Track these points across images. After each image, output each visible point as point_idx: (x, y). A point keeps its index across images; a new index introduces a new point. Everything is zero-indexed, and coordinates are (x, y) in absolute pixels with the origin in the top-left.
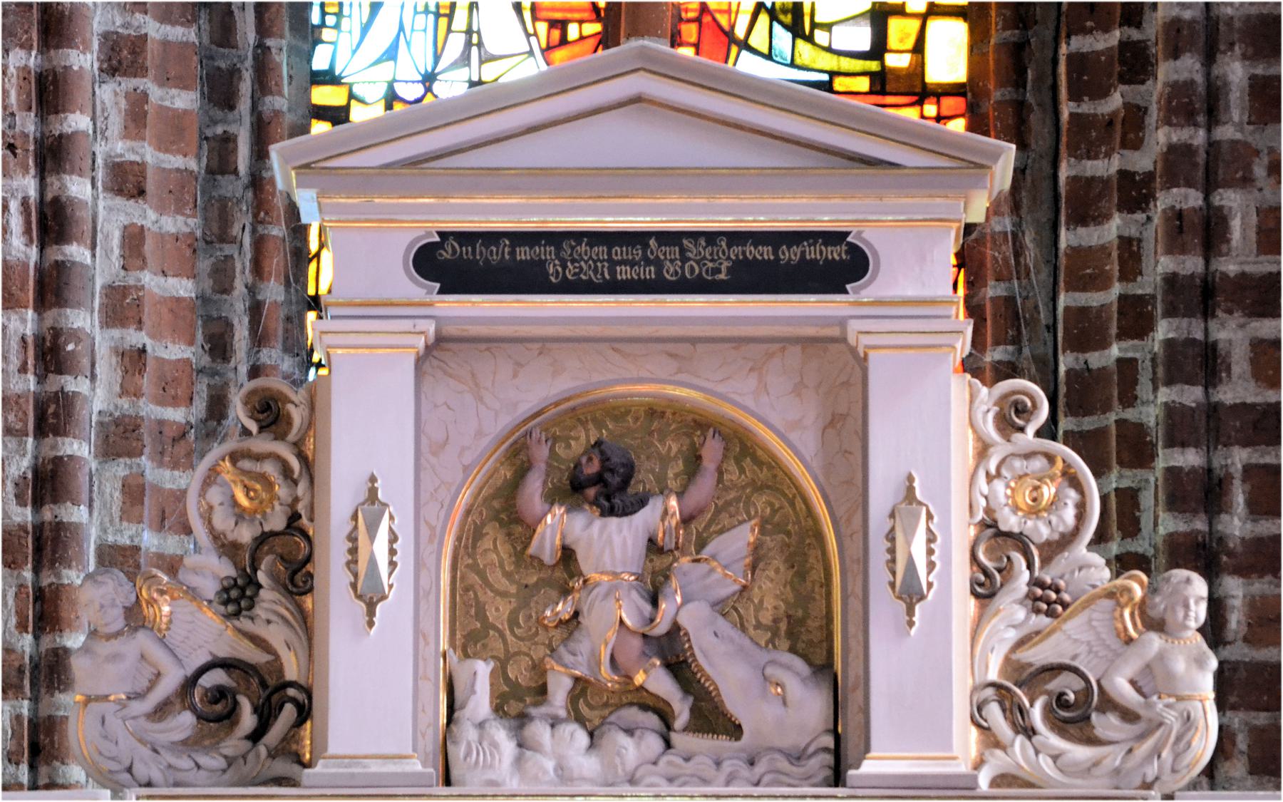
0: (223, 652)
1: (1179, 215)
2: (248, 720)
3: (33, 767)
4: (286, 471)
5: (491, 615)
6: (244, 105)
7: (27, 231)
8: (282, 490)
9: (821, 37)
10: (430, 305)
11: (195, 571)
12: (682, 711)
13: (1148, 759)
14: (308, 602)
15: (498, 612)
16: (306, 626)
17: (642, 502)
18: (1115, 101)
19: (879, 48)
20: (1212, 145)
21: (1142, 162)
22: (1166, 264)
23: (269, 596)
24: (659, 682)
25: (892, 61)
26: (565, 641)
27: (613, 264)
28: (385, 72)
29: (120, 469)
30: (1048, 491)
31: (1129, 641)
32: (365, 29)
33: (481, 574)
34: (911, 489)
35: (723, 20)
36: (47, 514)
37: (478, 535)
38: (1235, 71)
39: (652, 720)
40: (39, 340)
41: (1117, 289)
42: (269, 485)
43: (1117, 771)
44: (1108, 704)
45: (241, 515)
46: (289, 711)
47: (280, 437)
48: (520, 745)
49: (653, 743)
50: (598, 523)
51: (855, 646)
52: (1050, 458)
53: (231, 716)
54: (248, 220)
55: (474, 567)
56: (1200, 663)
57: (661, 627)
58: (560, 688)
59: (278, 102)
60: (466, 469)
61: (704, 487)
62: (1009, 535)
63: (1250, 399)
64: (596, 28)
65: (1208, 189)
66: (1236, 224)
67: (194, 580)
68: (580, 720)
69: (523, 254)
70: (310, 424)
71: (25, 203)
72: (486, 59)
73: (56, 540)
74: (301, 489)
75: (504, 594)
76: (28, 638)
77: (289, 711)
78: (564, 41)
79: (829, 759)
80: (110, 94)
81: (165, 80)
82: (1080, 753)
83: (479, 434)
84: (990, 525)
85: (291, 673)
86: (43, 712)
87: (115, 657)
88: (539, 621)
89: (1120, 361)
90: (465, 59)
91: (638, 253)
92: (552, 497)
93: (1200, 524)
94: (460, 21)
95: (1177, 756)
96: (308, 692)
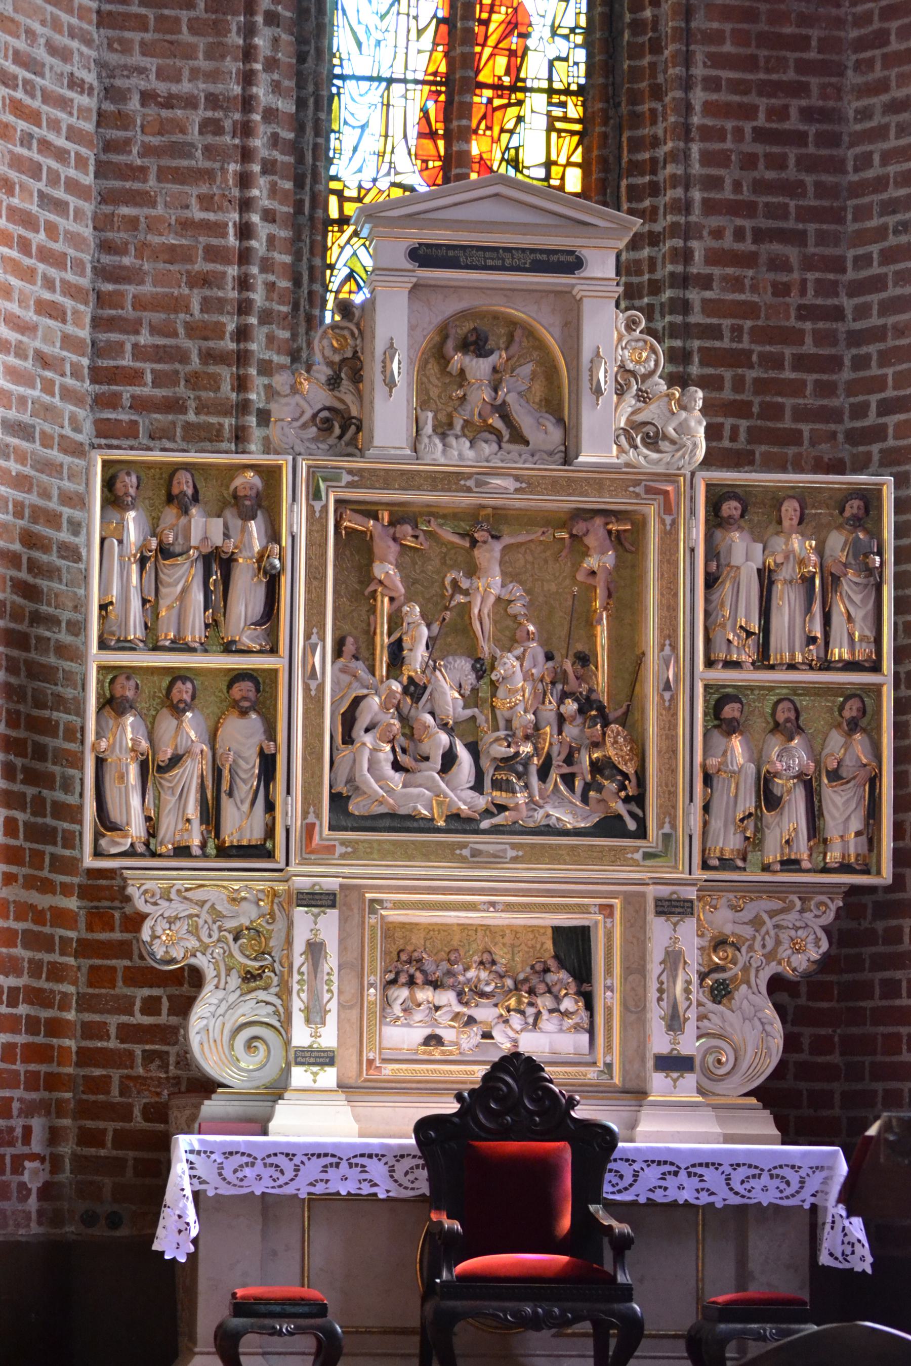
0: (328, 404)
1: (676, 249)
2: (337, 431)
3: (236, 445)
4: (353, 334)
5: (431, 394)
6: (308, 188)
7: (235, 235)
8: (350, 341)
9: (525, 171)
10: (414, 271)
11: (318, 372)
12: (506, 435)
13: (680, 459)
14: (361, 385)
15: (434, 392)
16: (359, 395)
17: (491, 352)
18: (647, 203)
19: (548, 177)
20: (687, 223)
21: (658, 227)
22: (670, 268)
23: (345, 383)
24: (495, 421)
25: (552, 182)
26: (460, 405)
27: (485, 259)
28: (359, 176)
29: (265, 329)
30: (644, 355)
31: (673, 414)
32: (351, 159)
33: (428, 378)
34: (598, 352)
35: (489, 163)
36: (242, 346)
37: (426, 362)
38: (697, 195)
39: (494, 437)
40: (239, 277)
41: (646, 277)
42: (346, 339)
43: (668, 463)
44: (665, 437)
45: (335, 350)
46: (353, 428)
47: (351, 321)
48: (444, 445)
49: (495, 447)
50: (475, 360)
51: (573, 412)
52: (645, 342)
53: (330, 429)
54: (308, 233)
55: (425, 375)
56: (700, 423)
57: (499, 401)
58: (458, 424)
59: (321, 187)
60: (425, 337)
61: (514, 348)
62: (629, 371)
63: (701, 321)
64: (440, 163)
65: (686, 240)
66: (697, 254)
67: (317, 375)
68: (465, 436)
69: (451, 253)
70: (362, 317)
71: (235, 224)
72: (397, 173)
73: (245, 356)
74: (358, 342)
75: (436, 386)
76: (235, 394)
77: (353, 428)
78: (427, 168)
79: (563, 455)
80: (262, 181)
81: (282, 178)
82: (654, 456)
83: (430, 323)
84: (622, 367)
85: (354, 412)
86: (240, 424)
87: (287, 404)
88: (450, 397)
89: (648, 304)
90: (388, 174)
91: (495, 255)
92: (457, 349)
93: (681, 369)
94: (387, 158)
95: (691, 458)
96: (360, 421)
